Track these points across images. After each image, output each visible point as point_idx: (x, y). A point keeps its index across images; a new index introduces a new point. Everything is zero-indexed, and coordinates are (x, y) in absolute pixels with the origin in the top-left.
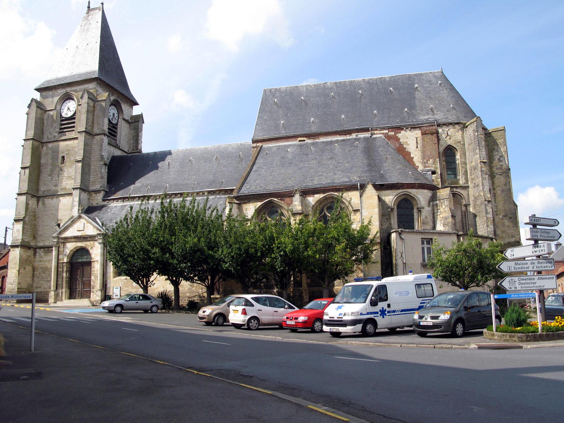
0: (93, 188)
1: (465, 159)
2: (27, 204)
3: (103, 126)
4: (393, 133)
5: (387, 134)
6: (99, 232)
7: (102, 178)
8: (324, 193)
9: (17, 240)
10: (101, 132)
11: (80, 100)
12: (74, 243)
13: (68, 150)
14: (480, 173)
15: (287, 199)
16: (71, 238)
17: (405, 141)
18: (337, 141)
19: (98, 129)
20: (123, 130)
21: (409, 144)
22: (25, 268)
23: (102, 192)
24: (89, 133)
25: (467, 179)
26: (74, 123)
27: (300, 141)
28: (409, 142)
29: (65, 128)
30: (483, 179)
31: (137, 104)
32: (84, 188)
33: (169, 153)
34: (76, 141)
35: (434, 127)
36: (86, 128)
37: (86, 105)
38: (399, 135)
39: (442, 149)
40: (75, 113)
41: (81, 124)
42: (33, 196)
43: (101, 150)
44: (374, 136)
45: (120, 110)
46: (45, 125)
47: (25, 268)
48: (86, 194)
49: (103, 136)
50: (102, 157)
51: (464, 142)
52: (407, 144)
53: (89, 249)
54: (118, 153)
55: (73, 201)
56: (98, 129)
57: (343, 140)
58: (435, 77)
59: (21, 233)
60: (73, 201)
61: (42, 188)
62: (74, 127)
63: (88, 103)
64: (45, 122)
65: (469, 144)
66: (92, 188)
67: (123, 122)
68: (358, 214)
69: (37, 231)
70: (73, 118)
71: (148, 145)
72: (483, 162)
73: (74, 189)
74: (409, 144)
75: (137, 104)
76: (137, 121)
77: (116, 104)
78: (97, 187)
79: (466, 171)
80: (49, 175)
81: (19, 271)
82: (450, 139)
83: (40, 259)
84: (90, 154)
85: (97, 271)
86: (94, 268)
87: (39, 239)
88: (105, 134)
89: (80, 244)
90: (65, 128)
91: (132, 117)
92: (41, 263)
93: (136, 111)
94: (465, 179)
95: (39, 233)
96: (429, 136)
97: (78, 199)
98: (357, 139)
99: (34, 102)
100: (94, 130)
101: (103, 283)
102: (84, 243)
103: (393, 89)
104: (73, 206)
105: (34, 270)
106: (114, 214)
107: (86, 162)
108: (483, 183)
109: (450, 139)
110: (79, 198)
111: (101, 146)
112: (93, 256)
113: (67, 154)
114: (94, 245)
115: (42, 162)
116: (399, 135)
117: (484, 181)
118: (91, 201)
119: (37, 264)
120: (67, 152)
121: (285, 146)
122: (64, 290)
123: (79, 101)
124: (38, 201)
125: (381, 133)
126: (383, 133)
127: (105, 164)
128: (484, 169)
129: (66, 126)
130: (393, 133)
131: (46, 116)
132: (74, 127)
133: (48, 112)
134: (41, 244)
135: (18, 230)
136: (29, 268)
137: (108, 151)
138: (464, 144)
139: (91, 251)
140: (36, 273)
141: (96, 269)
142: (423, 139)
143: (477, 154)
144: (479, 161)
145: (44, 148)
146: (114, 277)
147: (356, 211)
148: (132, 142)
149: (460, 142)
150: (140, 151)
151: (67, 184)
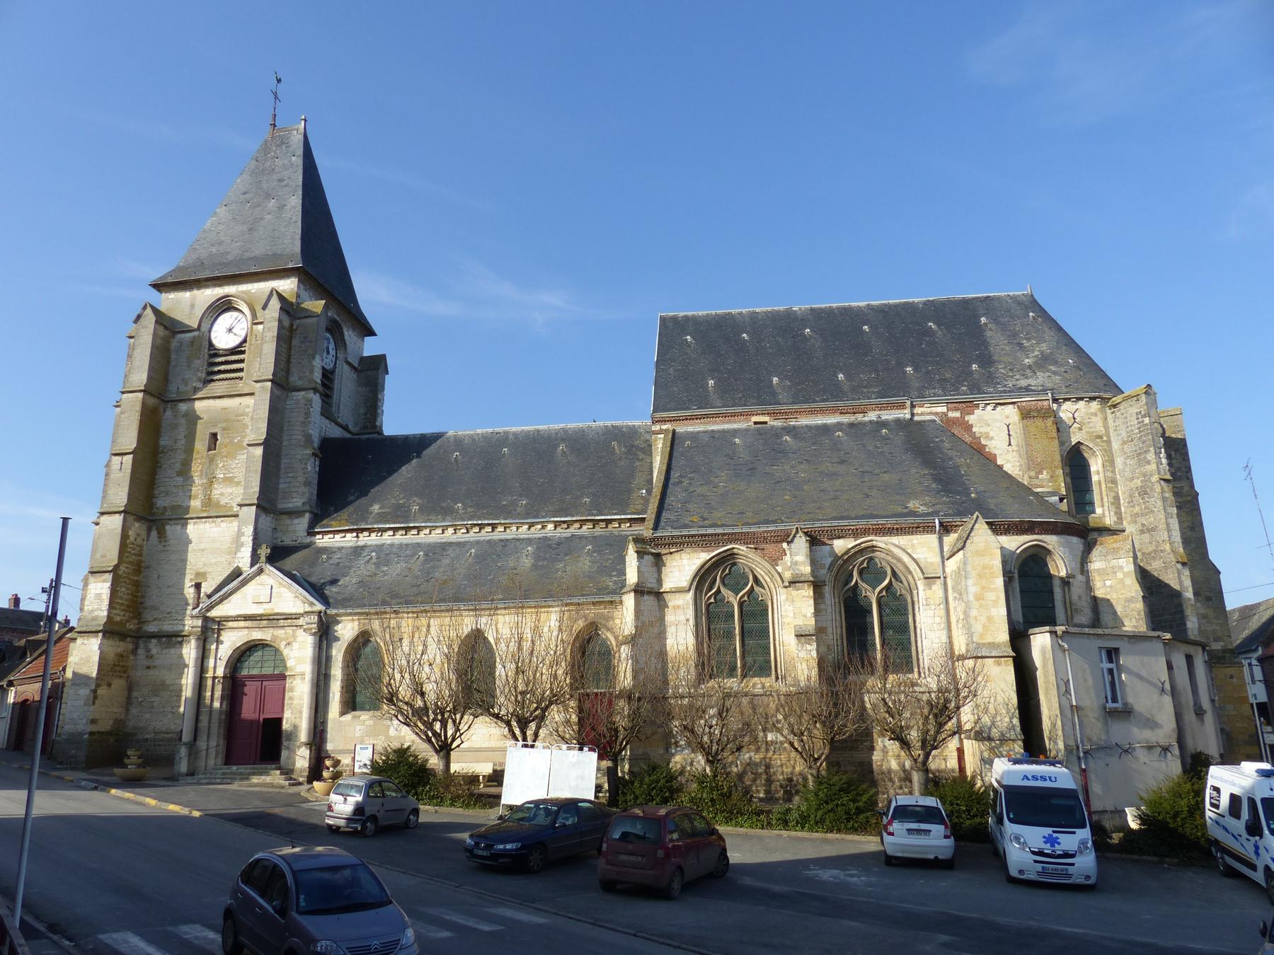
0: (286, 506)
1: (1113, 472)
2: (124, 536)
3: (312, 371)
4: (957, 414)
5: (945, 414)
6: (308, 609)
7: (307, 484)
8: (856, 537)
9: (95, 619)
10: (307, 386)
11: (260, 313)
12: (246, 632)
13: (226, 420)
14: (1159, 503)
15: (770, 548)
16: (236, 618)
17: (982, 430)
18: (839, 426)
19: (300, 378)
20: (346, 384)
21: (992, 438)
22: (109, 685)
23: (307, 515)
24: (282, 383)
25: (1119, 514)
26: (242, 361)
27: (756, 423)
28: (991, 434)
29: (220, 372)
30: (1168, 516)
31: (371, 333)
32: (268, 503)
33: (437, 436)
34: (249, 401)
35: (1045, 403)
36: (274, 374)
37: (276, 324)
38: (971, 419)
39: (1067, 448)
40: (245, 341)
41: (262, 362)
42: (139, 518)
43: (305, 424)
44: (916, 418)
45: (340, 342)
46: (173, 363)
47: (109, 685)
48: (269, 519)
49: (311, 395)
50: (308, 438)
51: (1109, 436)
52: (988, 437)
53: (282, 646)
54: (336, 432)
55: (240, 534)
56: (300, 378)
57: (852, 425)
58: (1020, 303)
59: (106, 602)
60: (240, 534)
61: (161, 502)
62: (241, 370)
63: (280, 321)
64: (173, 356)
65: (1124, 443)
66: (282, 505)
67: (346, 367)
68: (937, 587)
69: (143, 597)
70: (235, 351)
71: (397, 420)
72: (1165, 480)
73: (241, 505)
74: (992, 438)
75: (371, 333)
76: (373, 370)
77: (334, 329)
78: (297, 502)
79: (1117, 498)
80: (179, 474)
81: (95, 691)
82: (1080, 429)
83: (147, 663)
84: (281, 430)
85: (301, 699)
86: (292, 690)
87: (148, 615)
88: (315, 390)
89: (257, 635)
90: (220, 372)
91: (363, 360)
92: (151, 672)
93: (370, 347)
94: (1116, 513)
95: (149, 603)
96: (1039, 422)
97: (251, 529)
98: (881, 424)
99: (149, 310)
100: (291, 379)
101: (315, 727)
102: (271, 631)
103: (938, 324)
104: (238, 545)
105: (130, 689)
106: (338, 564)
107: (273, 448)
108: (1168, 524)
109: (1080, 429)
110: (255, 529)
111: (307, 414)
112: (289, 664)
113: (224, 429)
114: (294, 636)
115: (162, 443)
116: (971, 419)
117: (1171, 521)
118: (279, 535)
119: (139, 673)
120: (223, 425)
121: (724, 431)
122: (213, 743)
123: (254, 315)
124: (149, 530)
125: (931, 413)
126: (936, 414)
127: (938, 492)
128: (1167, 495)
129: (222, 368)
130: (957, 414)
131: (174, 344)
132: (241, 370)
133: (179, 336)
134: (151, 628)
135: (98, 596)
136: (119, 684)
137: (319, 427)
138: (1109, 442)
139: (286, 652)
140: (135, 694)
141: (296, 694)
142: (1025, 428)
143: (1149, 463)
144: (1155, 478)
145: (169, 413)
146: (343, 713)
147: (930, 579)
148: (362, 411)
149: (1100, 437)
150: (380, 433)
151: (222, 494)
